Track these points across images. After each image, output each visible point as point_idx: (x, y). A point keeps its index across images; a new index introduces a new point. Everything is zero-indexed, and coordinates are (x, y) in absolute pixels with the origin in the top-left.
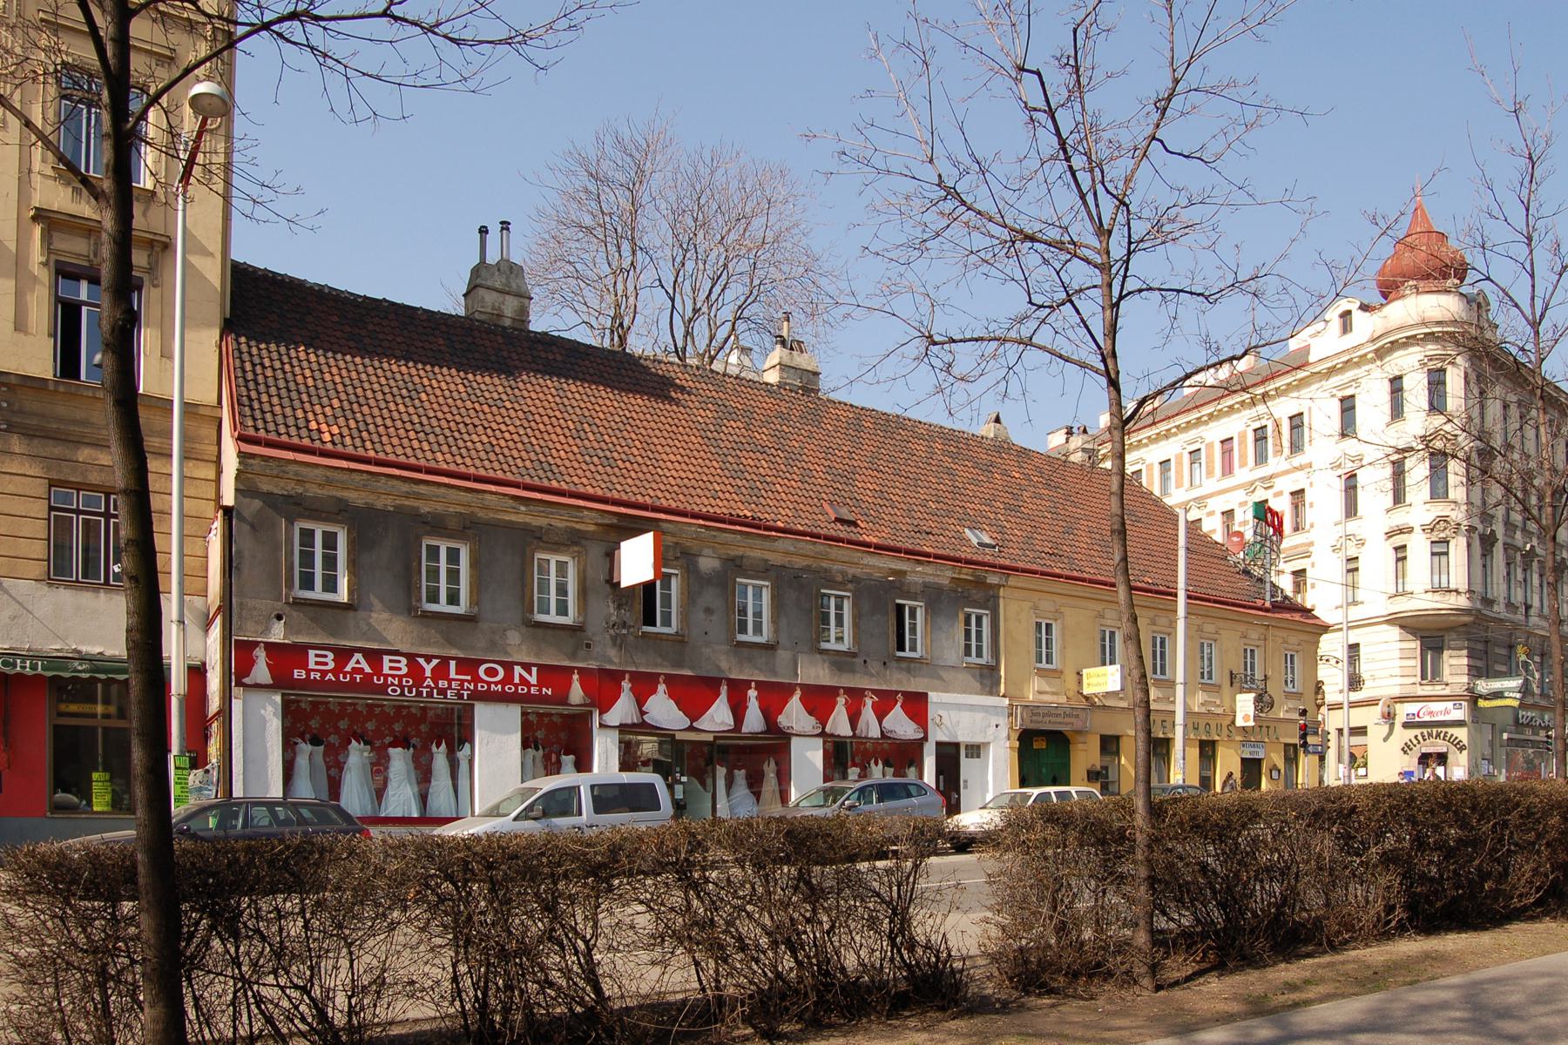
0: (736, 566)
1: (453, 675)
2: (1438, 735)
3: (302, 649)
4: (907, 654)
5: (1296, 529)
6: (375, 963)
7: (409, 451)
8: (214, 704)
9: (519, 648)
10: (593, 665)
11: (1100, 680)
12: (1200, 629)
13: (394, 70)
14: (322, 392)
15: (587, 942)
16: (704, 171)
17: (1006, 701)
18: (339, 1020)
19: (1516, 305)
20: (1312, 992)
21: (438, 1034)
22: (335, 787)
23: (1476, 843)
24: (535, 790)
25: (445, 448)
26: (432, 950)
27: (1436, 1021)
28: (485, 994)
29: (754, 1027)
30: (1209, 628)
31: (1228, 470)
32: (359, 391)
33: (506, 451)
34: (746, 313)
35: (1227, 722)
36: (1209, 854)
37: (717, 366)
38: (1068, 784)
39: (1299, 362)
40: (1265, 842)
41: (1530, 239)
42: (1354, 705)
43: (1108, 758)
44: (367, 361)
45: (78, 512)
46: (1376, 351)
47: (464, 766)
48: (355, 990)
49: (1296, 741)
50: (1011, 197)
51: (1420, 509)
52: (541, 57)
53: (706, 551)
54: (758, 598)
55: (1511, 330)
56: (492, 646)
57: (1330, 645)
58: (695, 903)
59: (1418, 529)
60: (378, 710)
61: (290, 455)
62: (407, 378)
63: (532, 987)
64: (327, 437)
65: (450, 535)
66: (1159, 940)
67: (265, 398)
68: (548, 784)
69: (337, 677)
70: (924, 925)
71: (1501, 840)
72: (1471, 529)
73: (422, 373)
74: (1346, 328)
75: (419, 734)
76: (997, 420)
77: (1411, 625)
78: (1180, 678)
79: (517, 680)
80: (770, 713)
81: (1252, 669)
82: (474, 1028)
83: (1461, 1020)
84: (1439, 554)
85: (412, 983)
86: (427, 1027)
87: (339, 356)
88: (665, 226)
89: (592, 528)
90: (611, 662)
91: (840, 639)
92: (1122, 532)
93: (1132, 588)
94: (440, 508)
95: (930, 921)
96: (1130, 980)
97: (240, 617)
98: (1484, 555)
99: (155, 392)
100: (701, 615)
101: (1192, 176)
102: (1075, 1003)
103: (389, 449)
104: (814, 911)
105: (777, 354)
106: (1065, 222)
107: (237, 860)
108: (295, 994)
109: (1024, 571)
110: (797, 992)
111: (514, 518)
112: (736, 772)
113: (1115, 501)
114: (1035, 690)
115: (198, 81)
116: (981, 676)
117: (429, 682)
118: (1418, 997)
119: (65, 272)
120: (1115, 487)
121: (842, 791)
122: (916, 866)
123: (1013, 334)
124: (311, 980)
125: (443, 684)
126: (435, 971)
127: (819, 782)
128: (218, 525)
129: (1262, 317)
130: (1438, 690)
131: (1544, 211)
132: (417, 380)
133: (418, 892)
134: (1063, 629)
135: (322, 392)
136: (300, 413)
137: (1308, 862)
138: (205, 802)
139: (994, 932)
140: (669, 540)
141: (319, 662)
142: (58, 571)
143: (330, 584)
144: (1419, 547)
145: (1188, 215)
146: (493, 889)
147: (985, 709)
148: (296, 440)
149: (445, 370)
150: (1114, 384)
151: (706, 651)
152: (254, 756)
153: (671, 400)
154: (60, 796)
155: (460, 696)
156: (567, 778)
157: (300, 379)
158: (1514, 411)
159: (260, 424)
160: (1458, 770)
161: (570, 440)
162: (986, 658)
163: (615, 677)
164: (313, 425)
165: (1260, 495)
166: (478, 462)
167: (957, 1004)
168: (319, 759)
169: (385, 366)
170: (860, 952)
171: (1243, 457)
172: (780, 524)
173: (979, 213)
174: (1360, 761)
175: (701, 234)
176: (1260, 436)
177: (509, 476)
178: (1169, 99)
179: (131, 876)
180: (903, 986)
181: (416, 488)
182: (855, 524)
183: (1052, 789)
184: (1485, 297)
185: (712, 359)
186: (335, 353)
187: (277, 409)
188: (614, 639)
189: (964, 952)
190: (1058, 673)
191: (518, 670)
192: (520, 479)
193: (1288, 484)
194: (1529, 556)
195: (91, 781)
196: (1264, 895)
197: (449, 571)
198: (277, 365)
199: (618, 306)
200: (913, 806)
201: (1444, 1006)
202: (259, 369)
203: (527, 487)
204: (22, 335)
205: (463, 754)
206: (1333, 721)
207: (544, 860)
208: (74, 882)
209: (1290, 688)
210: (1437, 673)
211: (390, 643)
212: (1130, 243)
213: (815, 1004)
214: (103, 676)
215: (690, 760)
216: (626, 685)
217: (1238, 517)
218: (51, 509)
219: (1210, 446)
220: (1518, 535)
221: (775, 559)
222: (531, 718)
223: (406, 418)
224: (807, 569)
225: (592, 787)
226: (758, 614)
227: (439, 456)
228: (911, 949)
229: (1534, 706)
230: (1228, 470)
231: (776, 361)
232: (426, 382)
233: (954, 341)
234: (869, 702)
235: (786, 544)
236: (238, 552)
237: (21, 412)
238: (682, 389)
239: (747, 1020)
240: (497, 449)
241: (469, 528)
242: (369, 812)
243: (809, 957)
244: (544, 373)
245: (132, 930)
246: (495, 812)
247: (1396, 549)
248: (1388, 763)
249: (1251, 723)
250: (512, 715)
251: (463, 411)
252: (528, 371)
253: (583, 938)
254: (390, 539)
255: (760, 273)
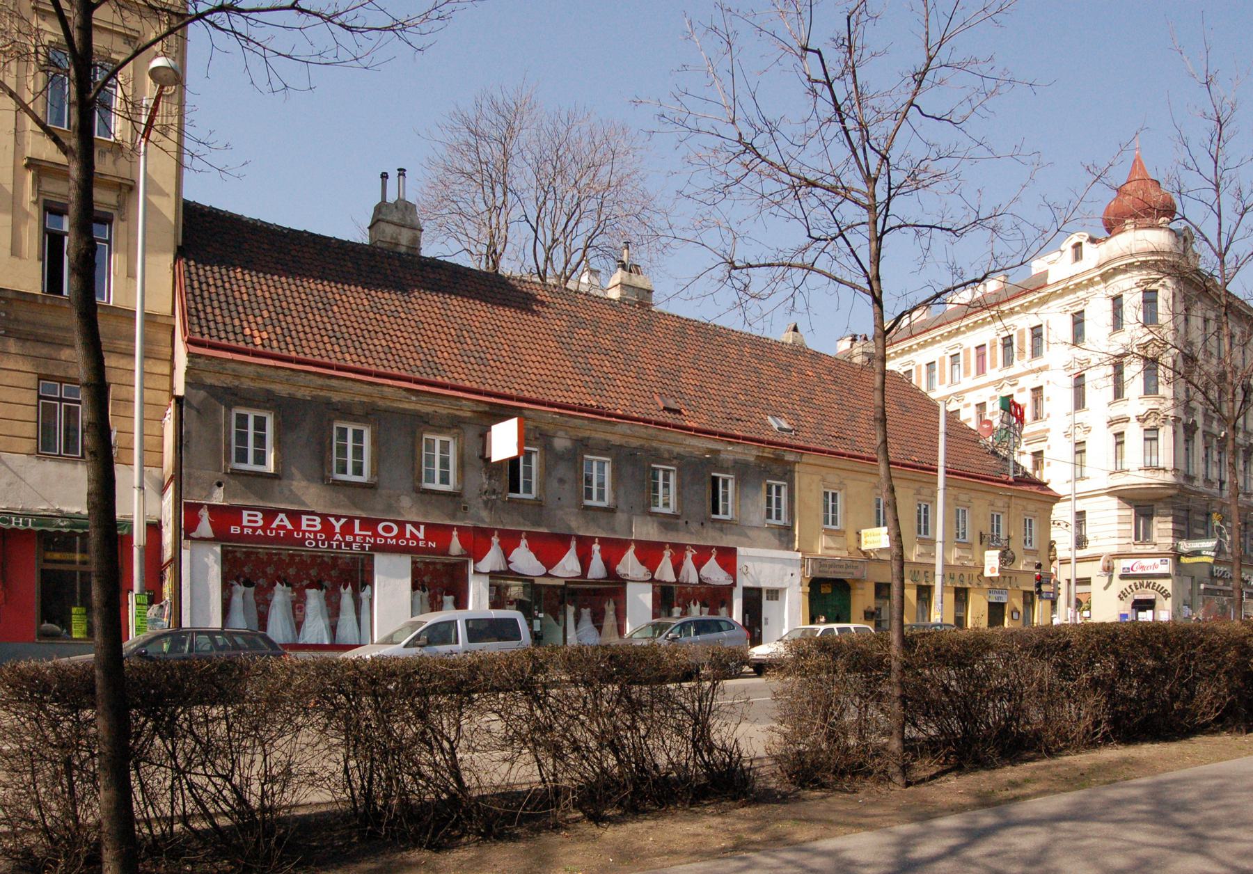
0: (583, 445)
1: (357, 531)
2: (1148, 585)
3: (238, 510)
4: (721, 516)
5: (1036, 418)
6: (283, 758)
7: (323, 352)
8: (168, 554)
9: (409, 509)
10: (468, 523)
11: (876, 538)
12: (956, 499)
13: (302, 50)
14: (255, 305)
15: (451, 743)
16: (562, 129)
17: (800, 555)
18: (255, 802)
19: (1206, 240)
20: (1029, 789)
21: (334, 814)
22: (263, 620)
23: (1167, 670)
24: (421, 623)
25: (352, 350)
26: (329, 748)
27: (1124, 813)
28: (370, 782)
29: (583, 811)
30: (963, 497)
31: (981, 370)
32: (284, 304)
33: (401, 353)
34: (595, 243)
35: (977, 573)
36: (949, 677)
37: (571, 285)
38: (849, 622)
39: (1039, 283)
40: (996, 669)
41: (1217, 186)
42: (1080, 560)
43: (881, 602)
44: (291, 280)
45: (61, 400)
46: (1101, 275)
47: (365, 603)
48: (268, 778)
49: (1033, 588)
50: (793, 151)
51: (1136, 402)
52: (418, 41)
53: (560, 433)
54: (601, 471)
55: (1207, 262)
56: (389, 508)
57: (1062, 512)
58: (538, 713)
59: (1133, 419)
60: (297, 559)
61: (229, 355)
62: (322, 294)
63: (407, 778)
64: (258, 341)
65: (356, 419)
66: (909, 746)
67: (209, 310)
68: (432, 618)
69: (265, 532)
70: (720, 732)
71: (1187, 669)
72: (1177, 419)
73: (334, 290)
74: (1078, 256)
75: (330, 577)
76: (795, 329)
77: (1127, 497)
78: (939, 537)
79: (408, 535)
80: (610, 563)
81: (998, 531)
82: (361, 810)
83: (1146, 812)
84: (1151, 439)
85: (313, 774)
86: (324, 809)
87: (268, 276)
88: (530, 173)
89: (469, 414)
90: (483, 521)
91: (666, 505)
92: (883, 420)
93: (889, 463)
94: (348, 398)
95: (726, 729)
96: (885, 778)
97: (189, 484)
98: (1187, 441)
99: (122, 304)
100: (555, 484)
101: (943, 134)
102: (841, 796)
103: (307, 350)
104: (633, 719)
105: (619, 276)
106: (838, 172)
107: (173, 675)
108: (219, 781)
109: (815, 450)
110: (618, 784)
111: (406, 406)
112: (583, 610)
113: (877, 395)
114: (823, 546)
115: (157, 56)
116: (780, 535)
117: (338, 536)
118: (1114, 793)
119: (52, 209)
120: (878, 383)
121: (667, 626)
122: (714, 686)
123: (797, 260)
124: (232, 771)
125: (349, 538)
126: (331, 764)
127: (649, 618)
128: (171, 411)
129: (999, 247)
130: (1148, 549)
131: (1229, 165)
132: (330, 295)
133: (317, 702)
134: (846, 497)
135: (255, 305)
136: (237, 322)
137: (1030, 685)
138: (158, 631)
139: (778, 739)
140: (530, 424)
141: (251, 521)
142: (45, 447)
143: (260, 458)
144: (1134, 434)
145: (935, 167)
146: (376, 702)
147: (783, 561)
148: (233, 343)
149: (353, 288)
150: (878, 301)
151: (560, 513)
152: (201, 593)
153: (533, 312)
154: (46, 625)
155: (363, 548)
156: (448, 613)
157: (237, 294)
158: (1212, 326)
159: (205, 330)
160: (1164, 613)
161: (452, 344)
162: (784, 520)
163: (486, 534)
164: (247, 331)
165: (1006, 391)
166: (378, 362)
167: (746, 795)
168: (251, 598)
169: (305, 284)
170: (668, 751)
171: (993, 360)
172: (619, 412)
173: (772, 164)
174: (1085, 605)
175: (559, 180)
176: (1008, 343)
177: (403, 373)
178: (924, 73)
179: (91, 690)
180: (703, 781)
181: (328, 382)
182: (679, 412)
183: (835, 626)
184: (1190, 233)
185: (567, 279)
186: (265, 274)
187: (219, 319)
188: (486, 503)
189: (752, 753)
190: (841, 533)
191: (409, 527)
192: (411, 375)
193: (1030, 382)
194: (1222, 443)
195: (71, 614)
196: (995, 712)
197: (355, 448)
198: (219, 283)
199: (492, 236)
200: (724, 638)
201: (1133, 800)
202: (204, 287)
203: (418, 382)
204: (16, 260)
205: (364, 595)
206: (1063, 574)
207: (417, 677)
208: (46, 692)
209: (1028, 546)
210: (1147, 535)
211: (306, 505)
212: (890, 189)
213: (632, 794)
214: (80, 531)
215: (546, 600)
216: (495, 540)
217: (989, 409)
218: (40, 397)
219: (967, 351)
220: (1215, 424)
221: (616, 440)
222: (419, 565)
223: (321, 326)
224: (642, 448)
225: (467, 621)
226: (601, 484)
227: (347, 357)
228: (710, 750)
229: (1226, 563)
230: (981, 370)
231: (618, 281)
232: (338, 297)
233: (751, 266)
234: (689, 555)
235: (624, 427)
236: (188, 432)
237: (16, 320)
238: (542, 303)
239: (578, 806)
240: (394, 351)
241: (370, 414)
242: (290, 640)
243: (628, 757)
244: (432, 290)
245: (93, 730)
246: (389, 640)
247: (1116, 435)
248: (1107, 607)
249: (997, 574)
250: (404, 563)
251: (367, 320)
252: (419, 288)
253: (448, 739)
254: (308, 423)
255: (606, 210)
